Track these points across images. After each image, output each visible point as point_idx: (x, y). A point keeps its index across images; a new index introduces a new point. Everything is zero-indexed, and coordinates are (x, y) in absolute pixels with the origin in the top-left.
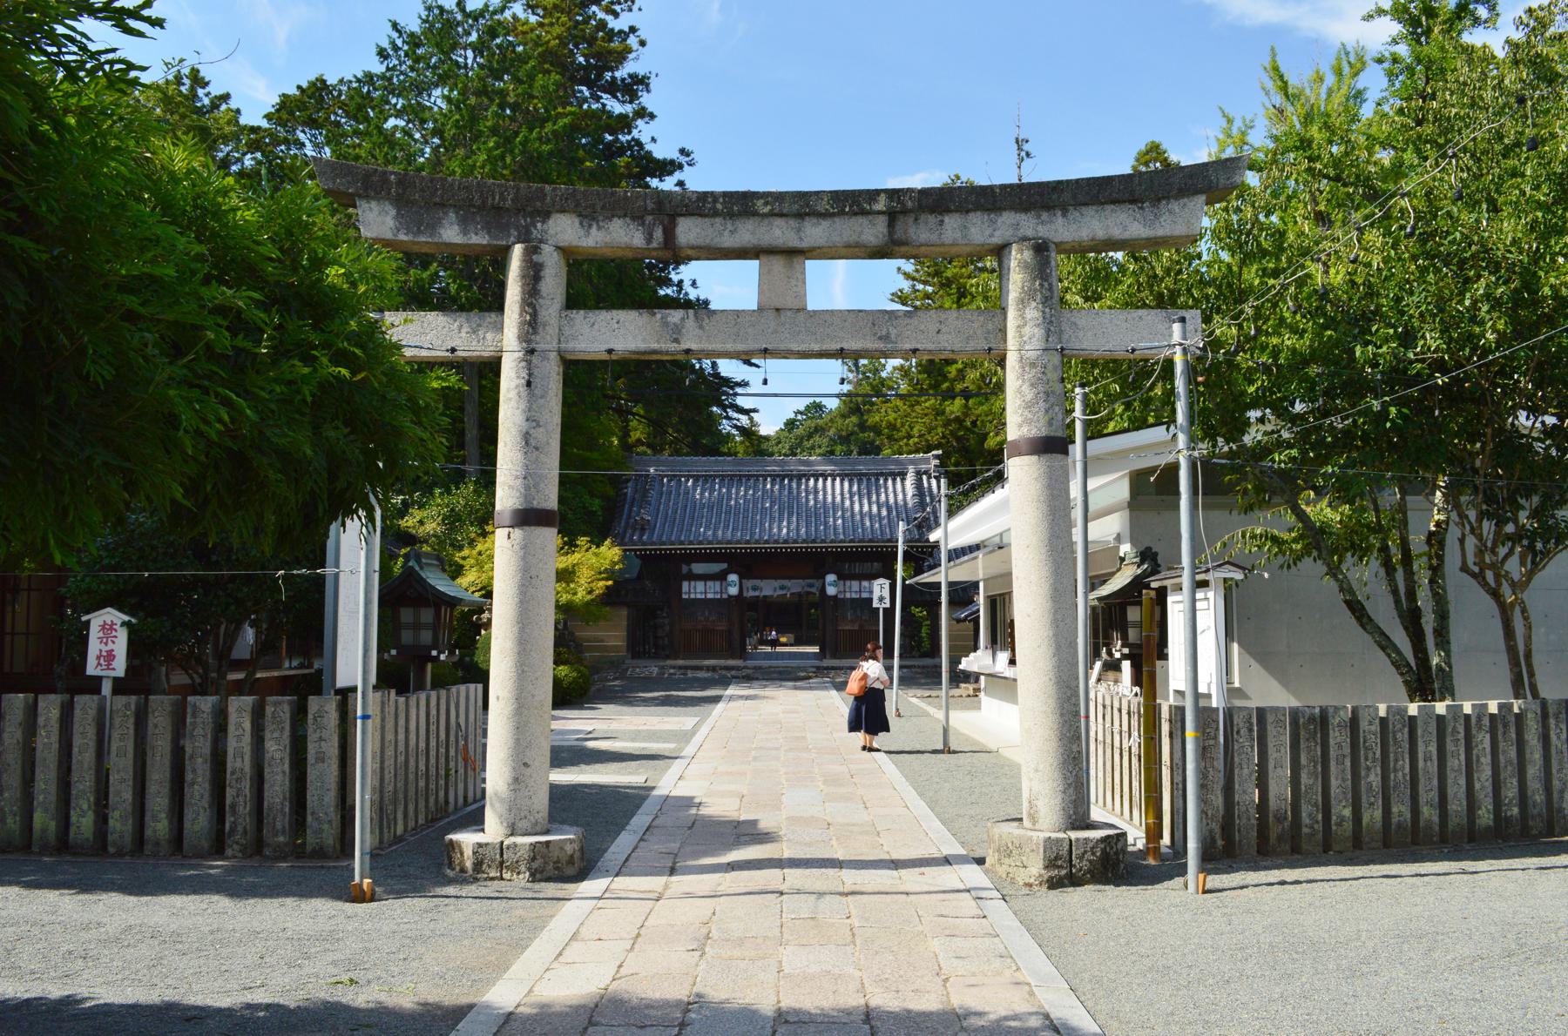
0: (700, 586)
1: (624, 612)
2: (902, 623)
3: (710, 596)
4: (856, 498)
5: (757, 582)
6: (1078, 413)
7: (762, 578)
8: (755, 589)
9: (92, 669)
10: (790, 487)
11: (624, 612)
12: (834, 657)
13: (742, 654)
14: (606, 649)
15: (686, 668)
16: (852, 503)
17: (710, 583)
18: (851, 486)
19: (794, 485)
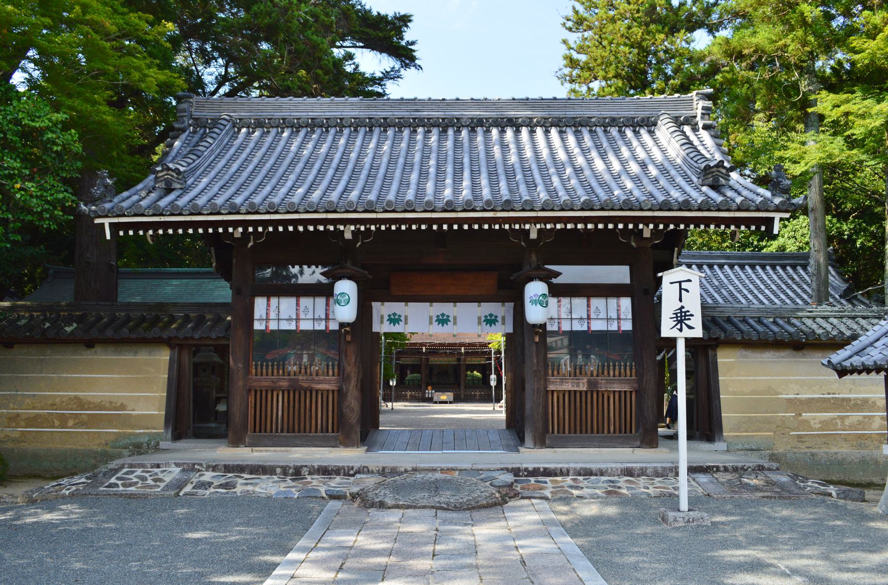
0: (287, 305)
1: (164, 356)
2: (689, 374)
3: (306, 326)
4: (594, 154)
5: (398, 307)
6: (26, 561)
7: (406, 299)
8: (394, 319)
9: (667, 329)
10: (473, 148)
11: (164, 356)
12: (541, 442)
13: (366, 429)
14: (126, 421)
15: (239, 469)
16: (590, 162)
17: (306, 302)
18: (580, 142)
19: (480, 138)
